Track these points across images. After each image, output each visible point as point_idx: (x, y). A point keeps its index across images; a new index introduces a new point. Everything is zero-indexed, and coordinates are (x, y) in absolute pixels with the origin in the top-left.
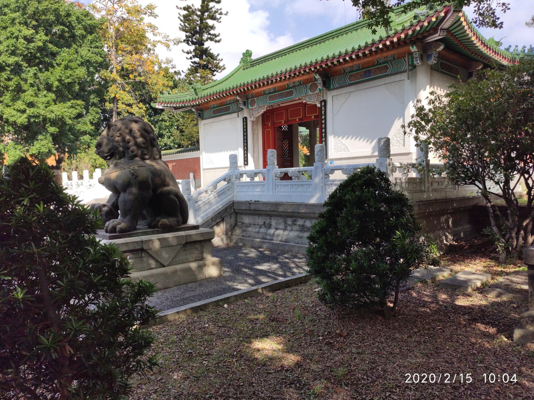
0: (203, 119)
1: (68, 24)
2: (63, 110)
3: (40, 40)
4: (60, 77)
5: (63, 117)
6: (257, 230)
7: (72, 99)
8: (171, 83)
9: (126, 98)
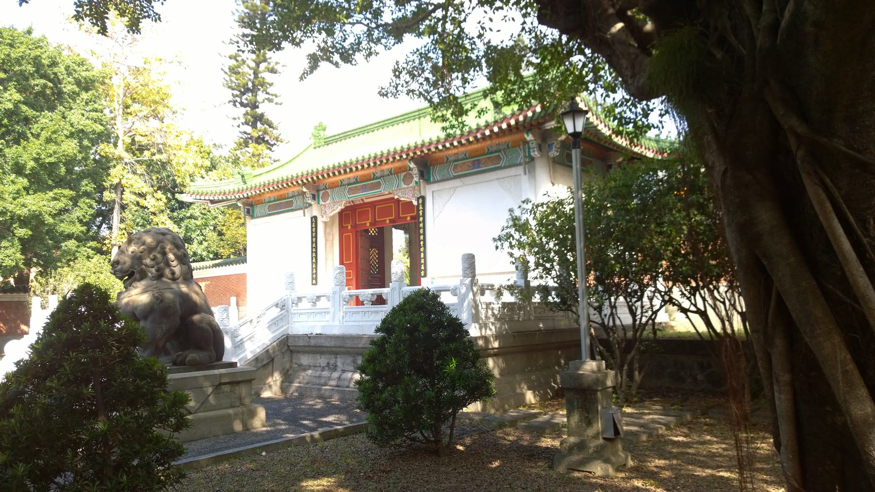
0: (253, 217)
1: (52, 76)
2: (38, 203)
3: (10, 100)
4: (38, 154)
5: (41, 214)
6: (318, 374)
7: (55, 187)
8: (208, 163)
9: (136, 185)
